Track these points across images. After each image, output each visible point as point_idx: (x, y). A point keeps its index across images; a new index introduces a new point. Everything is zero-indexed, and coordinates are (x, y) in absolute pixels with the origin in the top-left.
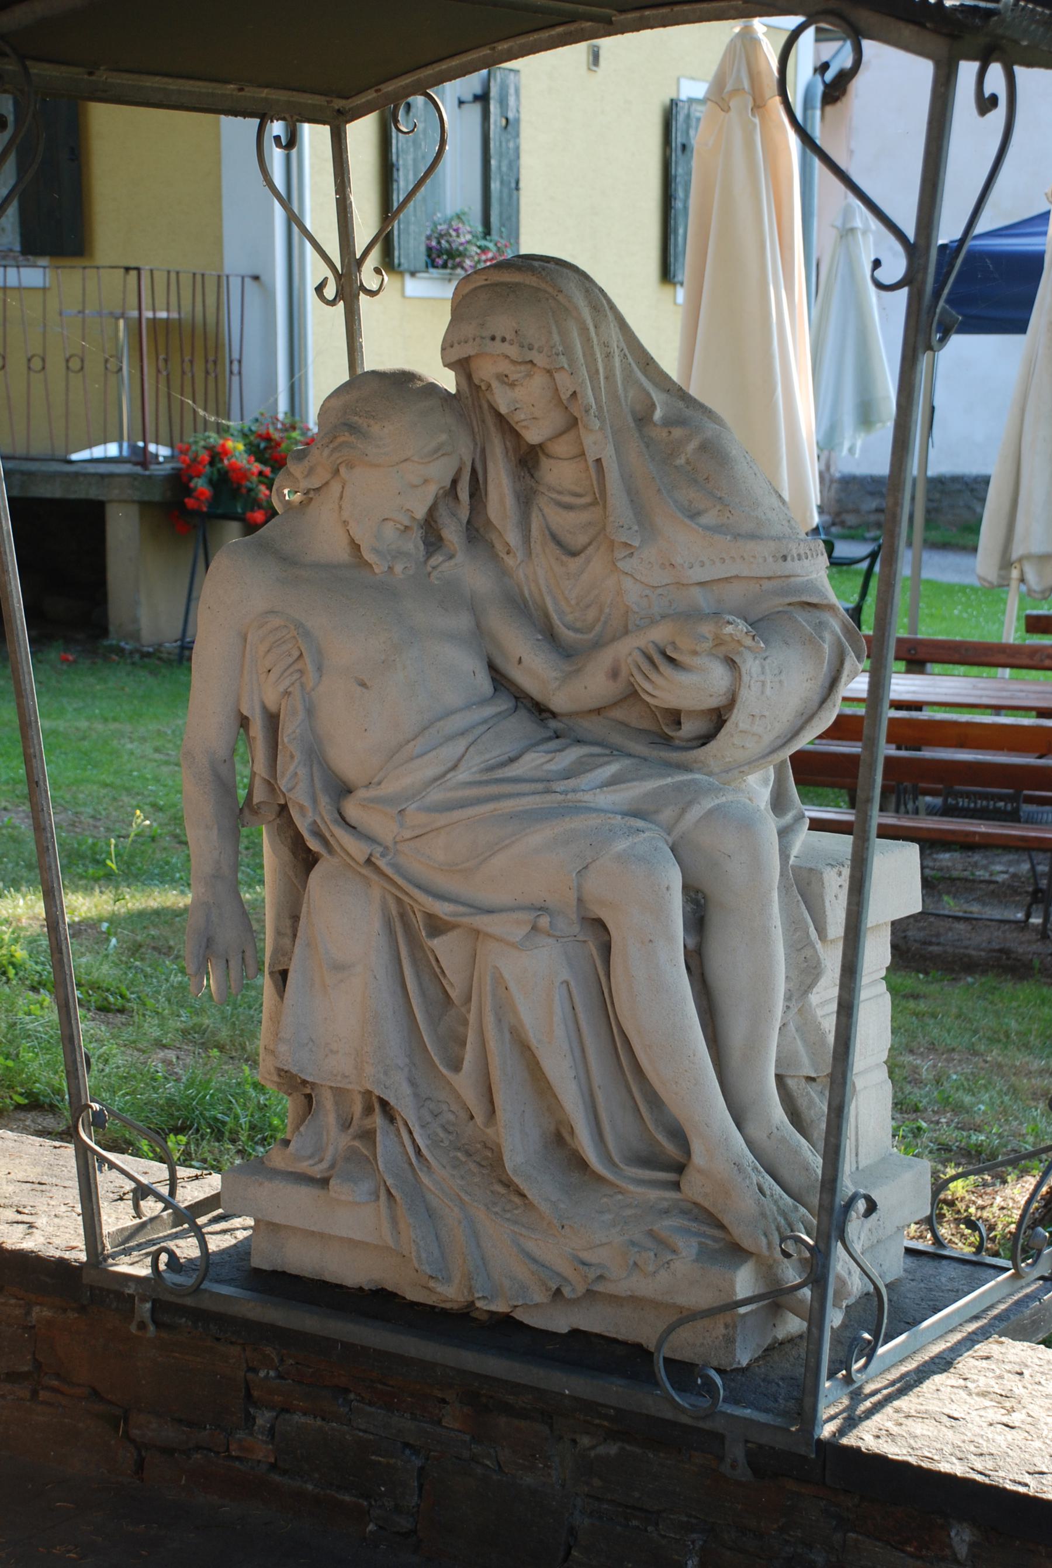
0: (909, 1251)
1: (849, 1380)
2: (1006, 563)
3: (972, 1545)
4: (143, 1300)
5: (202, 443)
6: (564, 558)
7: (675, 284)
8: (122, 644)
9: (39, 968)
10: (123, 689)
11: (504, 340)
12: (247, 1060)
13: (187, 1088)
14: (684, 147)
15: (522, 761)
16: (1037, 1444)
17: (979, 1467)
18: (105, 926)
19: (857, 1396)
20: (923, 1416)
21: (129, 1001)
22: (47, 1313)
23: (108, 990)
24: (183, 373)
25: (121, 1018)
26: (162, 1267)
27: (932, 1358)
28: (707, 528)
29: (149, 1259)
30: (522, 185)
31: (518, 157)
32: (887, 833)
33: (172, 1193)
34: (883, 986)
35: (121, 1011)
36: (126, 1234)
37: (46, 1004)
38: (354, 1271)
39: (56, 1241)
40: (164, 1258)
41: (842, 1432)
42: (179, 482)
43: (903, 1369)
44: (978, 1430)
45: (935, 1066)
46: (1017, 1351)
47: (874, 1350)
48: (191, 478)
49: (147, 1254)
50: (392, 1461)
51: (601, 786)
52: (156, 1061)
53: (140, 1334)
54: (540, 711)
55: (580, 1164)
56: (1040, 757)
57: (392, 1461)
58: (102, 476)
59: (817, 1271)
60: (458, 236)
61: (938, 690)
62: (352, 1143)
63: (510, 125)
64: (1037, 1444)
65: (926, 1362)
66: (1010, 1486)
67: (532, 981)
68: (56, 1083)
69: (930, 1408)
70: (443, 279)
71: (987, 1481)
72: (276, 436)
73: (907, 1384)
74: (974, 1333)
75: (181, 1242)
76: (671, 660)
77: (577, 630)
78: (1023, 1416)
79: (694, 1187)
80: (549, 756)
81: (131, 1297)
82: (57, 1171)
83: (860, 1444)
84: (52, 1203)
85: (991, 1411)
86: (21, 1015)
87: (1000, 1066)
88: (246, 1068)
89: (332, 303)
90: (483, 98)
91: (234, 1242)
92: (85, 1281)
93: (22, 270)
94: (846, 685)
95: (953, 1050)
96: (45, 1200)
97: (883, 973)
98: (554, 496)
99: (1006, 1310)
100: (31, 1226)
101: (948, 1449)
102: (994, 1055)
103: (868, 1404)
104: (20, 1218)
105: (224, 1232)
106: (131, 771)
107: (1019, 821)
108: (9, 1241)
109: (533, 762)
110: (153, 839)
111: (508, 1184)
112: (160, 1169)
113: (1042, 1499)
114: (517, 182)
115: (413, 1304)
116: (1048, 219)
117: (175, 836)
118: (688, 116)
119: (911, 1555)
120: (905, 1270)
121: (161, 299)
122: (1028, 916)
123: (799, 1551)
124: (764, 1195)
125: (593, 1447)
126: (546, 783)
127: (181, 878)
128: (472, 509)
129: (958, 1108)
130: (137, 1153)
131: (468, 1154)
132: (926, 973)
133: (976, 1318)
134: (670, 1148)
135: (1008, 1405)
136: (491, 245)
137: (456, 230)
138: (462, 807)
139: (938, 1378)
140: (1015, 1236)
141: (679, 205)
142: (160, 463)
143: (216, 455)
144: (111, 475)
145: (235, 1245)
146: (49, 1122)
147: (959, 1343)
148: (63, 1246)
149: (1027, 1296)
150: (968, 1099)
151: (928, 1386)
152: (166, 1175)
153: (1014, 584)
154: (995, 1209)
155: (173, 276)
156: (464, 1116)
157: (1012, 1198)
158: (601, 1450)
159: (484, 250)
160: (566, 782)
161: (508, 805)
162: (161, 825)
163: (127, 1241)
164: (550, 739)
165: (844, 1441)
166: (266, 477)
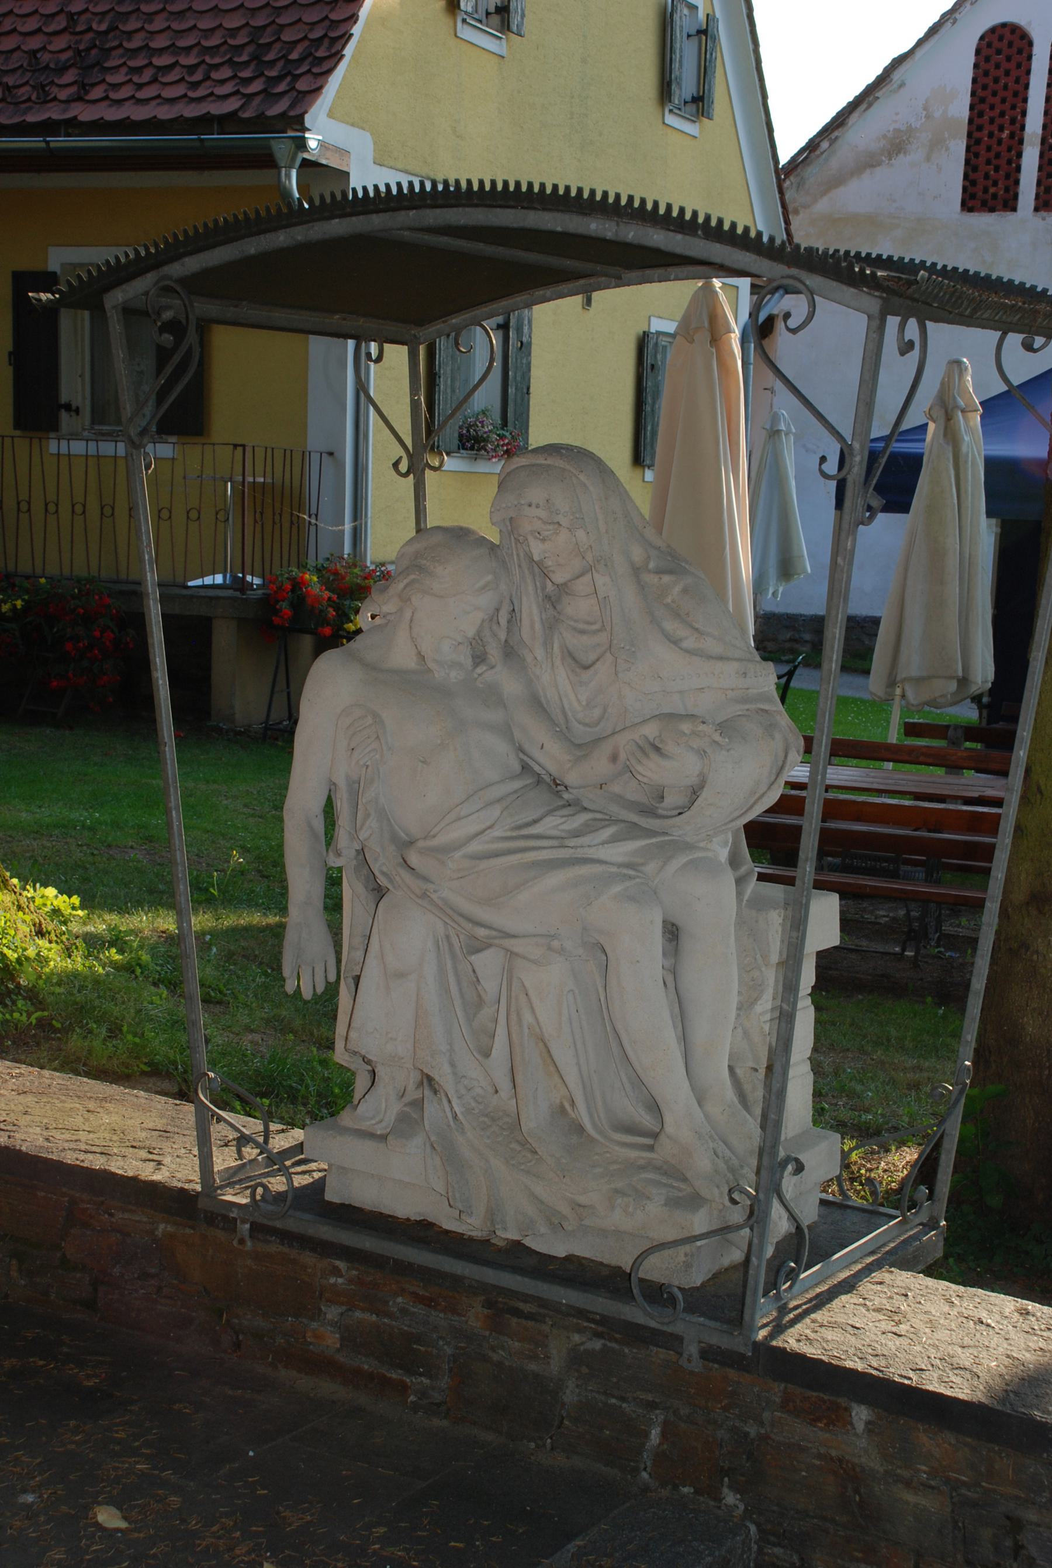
0: (823, 1202)
1: (778, 1297)
2: (892, 683)
3: (868, 1423)
4: (244, 1222)
5: (286, 576)
6: (578, 670)
7: (644, 467)
8: (221, 725)
9: (158, 968)
10: (221, 759)
11: (537, 506)
12: (314, 1043)
13: (270, 1063)
14: (653, 366)
15: (542, 822)
16: (918, 1348)
17: (875, 1365)
18: (208, 937)
19: (783, 1310)
20: (832, 1325)
21: (225, 995)
22: (170, 1229)
23: (210, 987)
24: (274, 523)
25: (218, 1009)
26: (258, 1197)
27: (839, 1283)
28: (687, 651)
29: (249, 1191)
30: (532, 390)
31: (529, 370)
32: (819, 885)
33: (266, 1141)
34: (809, 1000)
35: (219, 1003)
36: (231, 1171)
37: (164, 996)
38: (405, 1206)
39: (179, 1175)
40: (260, 1190)
41: (772, 1336)
42: (268, 602)
43: (818, 1290)
44: (874, 1337)
45: (834, 1062)
46: (903, 1278)
47: (798, 1275)
48: (277, 602)
49: (247, 1188)
50: (430, 1349)
51: (603, 843)
52: (247, 1041)
53: (241, 1247)
54: (556, 785)
55: (580, 1129)
56: (915, 830)
57: (430, 1349)
58: (211, 598)
59: (757, 1216)
60: (483, 427)
61: (840, 777)
62: (405, 1109)
63: (525, 347)
64: (918, 1348)
65: (835, 1285)
66: (897, 1379)
67: (549, 991)
68: (171, 1055)
69: (839, 1320)
70: (470, 458)
71: (881, 1375)
72: (342, 571)
73: (821, 1301)
74: (871, 1264)
75: (272, 1180)
76: (657, 749)
77: (586, 725)
78: (908, 1327)
79: (666, 1150)
80: (564, 819)
81: (235, 1219)
82: (178, 1122)
83: (786, 1345)
84: (175, 1146)
85: (883, 1323)
86: (145, 1004)
87: (883, 1063)
88: (315, 1049)
89: (405, 475)
90: (504, 327)
91: (311, 1180)
92: (199, 1206)
93: (100, 443)
94: (789, 771)
95: (848, 1050)
96: (169, 1144)
97: (809, 991)
98: (572, 623)
99: (893, 1248)
100: (159, 1163)
101: (852, 1351)
102: (878, 1054)
103: (791, 1316)
104: (151, 1157)
105: (304, 1173)
106: (226, 821)
107: (898, 878)
108: (143, 1174)
109: (551, 825)
110: (242, 873)
111: (524, 1143)
112: (255, 1124)
113: (921, 1389)
114: (528, 389)
115: (447, 1232)
116: (926, 430)
117: (259, 871)
118: (656, 344)
119: (821, 1429)
120: (819, 1216)
121: (259, 468)
122: (904, 950)
123: (737, 1425)
124: (718, 1157)
125: (582, 1343)
126: (561, 841)
127: (263, 903)
128: (509, 631)
129: (852, 1094)
130: (233, 1110)
131: (493, 1120)
132: (827, 992)
133: (872, 1253)
134: (647, 1120)
135: (896, 1318)
136: (507, 434)
137: (482, 422)
138: (497, 856)
139: (844, 1298)
140: (899, 1191)
141: (648, 408)
142: (254, 590)
143: (297, 584)
144: (218, 598)
145: (312, 1183)
146: (166, 1085)
147: (860, 1271)
148: (184, 1178)
149: (910, 1237)
150: (859, 1088)
151: (836, 1303)
152: (261, 1128)
153: (897, 699)
154: (880, 1171)
155: (269, 451)
156: (491, 1090)
157: (902, 1160)
158: (589, 1345)
159: (502, 437)
160: (576, 839)
161: (531, 856)
162: (248, 862)
163: (232, 1178)
164: (564, 806)
165: (774, 1343)
166: (334, 601)
